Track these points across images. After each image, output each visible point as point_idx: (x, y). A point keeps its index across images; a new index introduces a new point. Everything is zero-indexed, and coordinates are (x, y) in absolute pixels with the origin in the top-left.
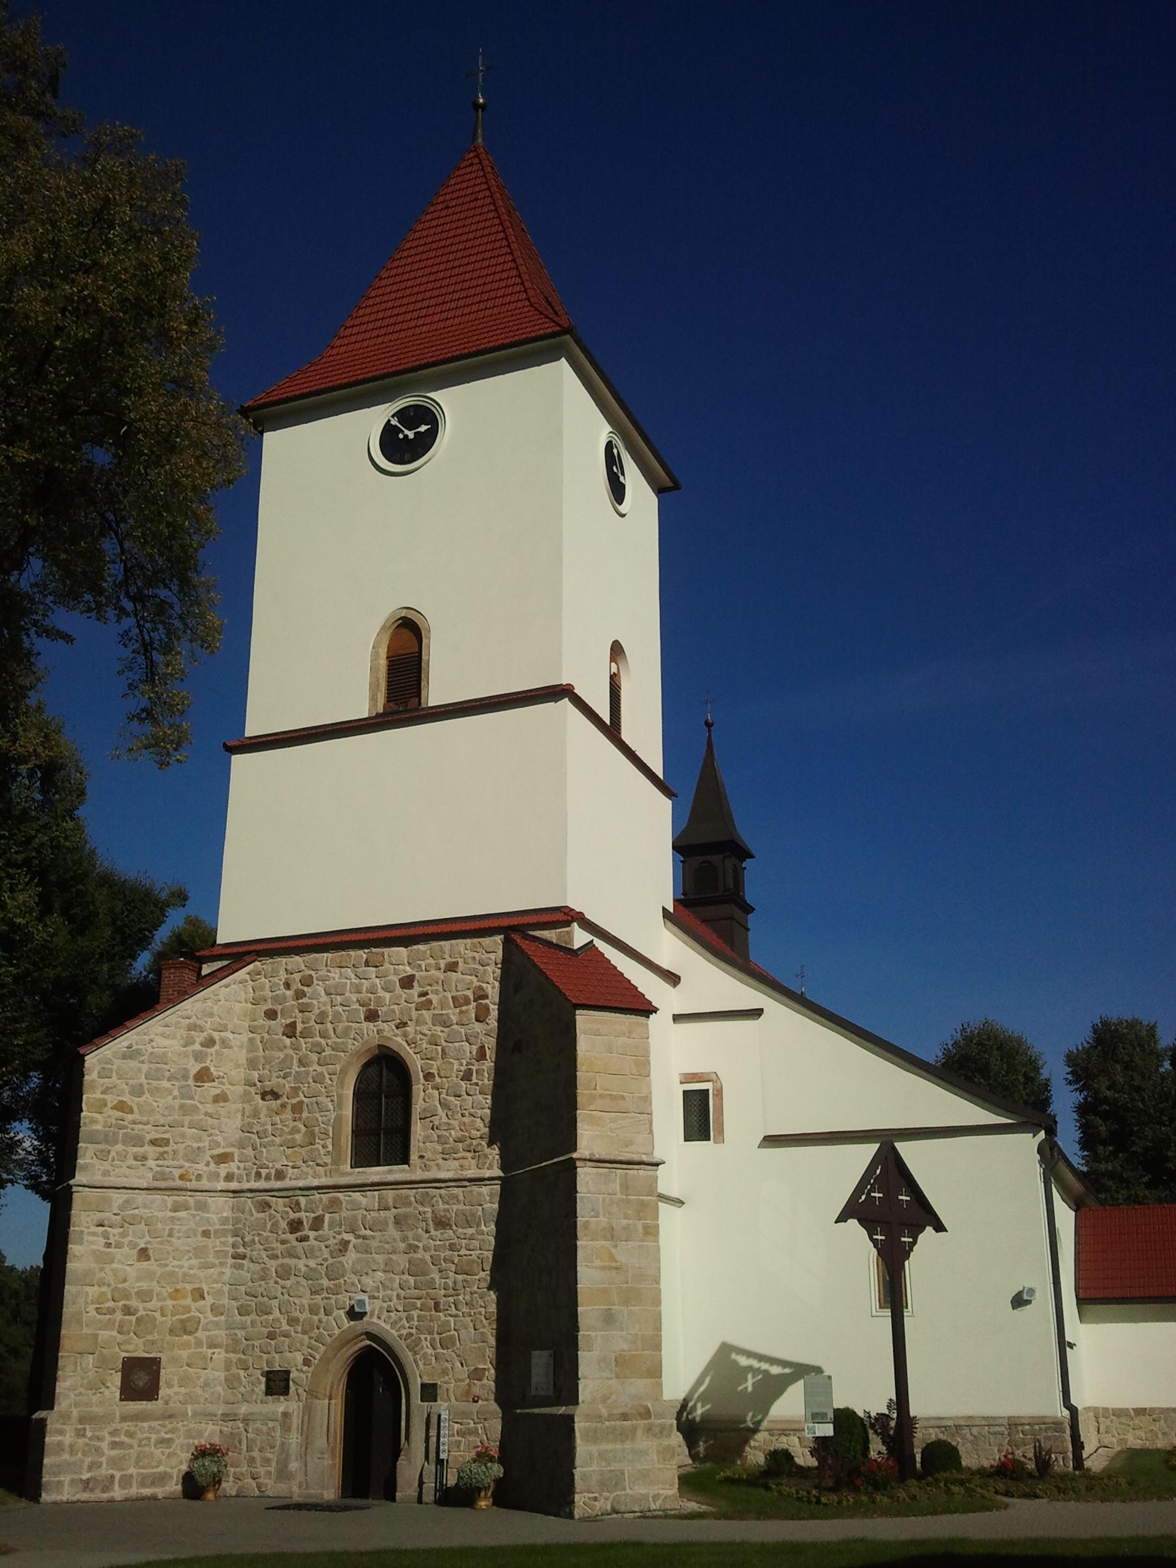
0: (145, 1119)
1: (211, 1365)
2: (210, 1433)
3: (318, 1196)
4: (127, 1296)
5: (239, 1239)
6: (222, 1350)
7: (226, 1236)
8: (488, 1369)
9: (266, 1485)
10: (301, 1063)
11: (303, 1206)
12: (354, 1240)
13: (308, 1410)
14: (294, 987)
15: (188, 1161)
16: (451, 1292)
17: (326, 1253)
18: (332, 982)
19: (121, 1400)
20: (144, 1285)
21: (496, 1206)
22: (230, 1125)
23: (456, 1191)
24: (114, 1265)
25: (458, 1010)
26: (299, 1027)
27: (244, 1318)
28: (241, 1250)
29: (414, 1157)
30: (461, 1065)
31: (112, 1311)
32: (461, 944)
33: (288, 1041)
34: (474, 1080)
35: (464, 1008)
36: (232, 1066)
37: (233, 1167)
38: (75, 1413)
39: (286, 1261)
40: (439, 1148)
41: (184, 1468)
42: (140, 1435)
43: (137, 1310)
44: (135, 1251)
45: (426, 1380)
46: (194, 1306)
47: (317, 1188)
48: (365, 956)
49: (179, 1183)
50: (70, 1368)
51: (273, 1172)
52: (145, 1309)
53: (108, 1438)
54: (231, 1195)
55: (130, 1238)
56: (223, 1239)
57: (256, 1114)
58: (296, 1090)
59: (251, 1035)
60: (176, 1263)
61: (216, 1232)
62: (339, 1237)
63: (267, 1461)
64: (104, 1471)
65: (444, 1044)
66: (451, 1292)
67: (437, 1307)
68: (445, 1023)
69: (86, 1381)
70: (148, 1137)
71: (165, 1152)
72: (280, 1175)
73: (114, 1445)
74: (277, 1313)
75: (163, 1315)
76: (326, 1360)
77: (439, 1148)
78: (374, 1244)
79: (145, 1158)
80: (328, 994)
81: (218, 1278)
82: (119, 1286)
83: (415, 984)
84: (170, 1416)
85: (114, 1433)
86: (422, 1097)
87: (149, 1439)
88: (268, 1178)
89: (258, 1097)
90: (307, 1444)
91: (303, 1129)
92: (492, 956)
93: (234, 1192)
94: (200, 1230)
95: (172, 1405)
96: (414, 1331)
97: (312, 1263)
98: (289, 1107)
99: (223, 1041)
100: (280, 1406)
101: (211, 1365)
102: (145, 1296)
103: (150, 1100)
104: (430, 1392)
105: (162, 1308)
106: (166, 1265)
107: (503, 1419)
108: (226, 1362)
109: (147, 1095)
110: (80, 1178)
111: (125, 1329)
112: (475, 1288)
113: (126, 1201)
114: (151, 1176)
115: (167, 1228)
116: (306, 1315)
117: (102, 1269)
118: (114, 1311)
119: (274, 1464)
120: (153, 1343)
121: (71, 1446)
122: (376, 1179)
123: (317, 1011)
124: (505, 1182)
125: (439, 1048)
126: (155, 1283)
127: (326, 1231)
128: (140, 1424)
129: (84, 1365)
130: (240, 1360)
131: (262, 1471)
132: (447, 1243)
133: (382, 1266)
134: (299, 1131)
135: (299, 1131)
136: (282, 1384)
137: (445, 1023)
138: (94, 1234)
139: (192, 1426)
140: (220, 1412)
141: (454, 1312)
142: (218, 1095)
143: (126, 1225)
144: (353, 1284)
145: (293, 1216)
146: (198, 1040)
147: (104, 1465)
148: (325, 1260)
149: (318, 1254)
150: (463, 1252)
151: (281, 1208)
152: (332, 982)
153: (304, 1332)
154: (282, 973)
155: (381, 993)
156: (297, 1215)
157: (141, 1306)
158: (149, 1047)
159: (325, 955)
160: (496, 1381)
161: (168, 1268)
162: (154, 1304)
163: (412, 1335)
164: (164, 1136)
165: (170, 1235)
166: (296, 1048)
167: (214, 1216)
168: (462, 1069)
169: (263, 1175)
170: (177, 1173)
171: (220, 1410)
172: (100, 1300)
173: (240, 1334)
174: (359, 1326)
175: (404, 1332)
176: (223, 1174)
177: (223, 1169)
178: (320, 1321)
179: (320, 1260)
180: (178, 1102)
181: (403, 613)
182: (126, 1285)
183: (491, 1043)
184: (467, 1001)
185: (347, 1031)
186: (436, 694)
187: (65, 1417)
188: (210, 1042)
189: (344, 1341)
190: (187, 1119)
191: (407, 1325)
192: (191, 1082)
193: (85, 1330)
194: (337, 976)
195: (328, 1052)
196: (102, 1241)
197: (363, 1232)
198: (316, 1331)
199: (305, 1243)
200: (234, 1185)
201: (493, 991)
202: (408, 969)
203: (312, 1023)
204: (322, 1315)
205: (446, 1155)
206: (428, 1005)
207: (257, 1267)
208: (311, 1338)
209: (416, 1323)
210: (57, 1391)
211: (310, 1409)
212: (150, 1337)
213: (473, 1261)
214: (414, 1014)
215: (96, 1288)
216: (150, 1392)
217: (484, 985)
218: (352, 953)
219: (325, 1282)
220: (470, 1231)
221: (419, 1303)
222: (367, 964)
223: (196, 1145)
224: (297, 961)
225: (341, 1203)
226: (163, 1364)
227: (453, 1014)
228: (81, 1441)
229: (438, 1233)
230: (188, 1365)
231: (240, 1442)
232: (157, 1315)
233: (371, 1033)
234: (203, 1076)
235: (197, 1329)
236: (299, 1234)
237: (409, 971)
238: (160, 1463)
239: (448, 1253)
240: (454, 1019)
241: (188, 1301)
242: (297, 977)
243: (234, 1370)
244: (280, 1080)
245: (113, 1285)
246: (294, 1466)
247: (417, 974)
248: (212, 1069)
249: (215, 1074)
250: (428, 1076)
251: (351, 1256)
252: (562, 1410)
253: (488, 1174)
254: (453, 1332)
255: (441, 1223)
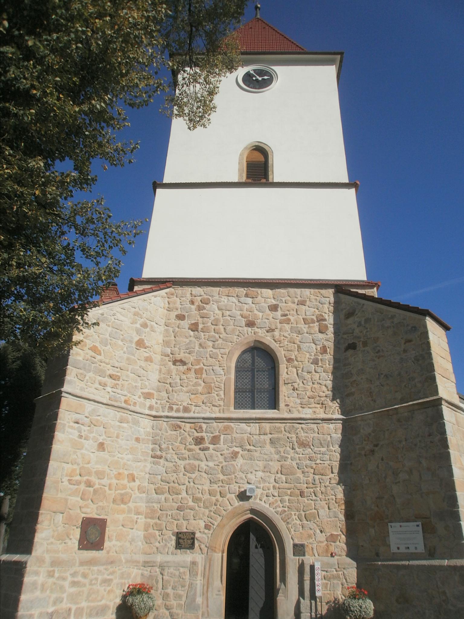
0: (107, 361)
1: (136, 527)
2: (135, 576)
3: (215, 424)
4: (89, 473)
5: (157, 446)
6: (143, 517)
7: (148, 444)
8: (340, 535)
9: (178, 615)
10: (200, 345)
11: (204, 429)
12: (241, 452)
13: (209, 561)
14: (196, 304)
15: (129, 392)
16: (311, 485)
17: (221, 459)
18: (222, 303)
19: (79, 549)
20: (100, 467)
21: (340, 435)
22: (154, 375)
23: (315, 426)
24: (83, 451)
25: (307, 326)
26: (201, 326)
27: (160, 496)
28: (159, 453)
29: (282, 405)
30: (311, 355)
31: (78, 483)
32: (307, 292)
33: (192, 333)
34: (320, 364)
35: (311, 325)
36: (156, 339)
37: (153, 402)
38: (48, 558)
39: (192, 462)
40: (299, 401)
41: (118, 601)
42: (91, 577)
43: (94, 484)
44: (96, 444)
45: (297, 542)
46: (128, 485)
47: (215, 419)
48: (245, 292)
49: (123, 405)
50: (46, 523)
51: (181, 407)
52: (99, 484)
53: (70, 579)
54: (152, 418)
55: (94, 435)
56: (147, 445)
57: (169, 372)
58: (198, 362)
59: (166, 328)
60: (120, 455)
61: (143, 439)
62: (231, 449)
63: (180, 597)
64: (65, 605)
65: (299, 343)
66: (311, 485)
67: (302, 494)
68: (299, 333)
69: (56, 534)
70: (108, 373)
71: (118, 384)
72: (186, 410)
73: (74, 584)
74: (184, 494)
75: (110, 489)
76: (221, 526)
77: (299, 401)
78: (257, 454)
79: (105, 385)
80: (219, 309)
81: (143, 467)
82: (86, 466)
83: (279, 309)
84: (112, 562)
85: (74, 575)
86: (285, 372)
87: (96, 579)
88: (178, 410)
89: (170, 364)
90: (208, 584)
91: (203, 384)
92: (328, 299)
93: (155, 417)
94: (135, 436)
95: (111, 554)
96: (286, 509)
97: (211, 464)
98: (193, 370)
99: (152, 327)
100: (187, 557)
101: (136, 527)
102: (100, 475)
103: (111, 350)
104: (299, 549)
105: (110, 485)
106: (114, 456)
107: (357, 568)
108: (145, 525)
109: (109, 346)
110: (66, 388)
111: (86, 497)
112: (328, 483)
113: (94, 410)
114: (108, 397)
115: (116, 432)
116: (207, 496)
117: (75, 453)
118: (80, 483)
119: (184, 599)
120: (103, 508)
121: (43, 585)
122: (258, 416)
123: (212, 318)
124: (345, 423)
125: (296, 345)
126: (107, 467)
127: (221, 445)
128: (92, 568)
129: (56, 521)
130: (156, 524)
131: (174, 603)
132: (308, 456)
133: (262, 468)
134: (200, 385)
135: (200, 385)
136: (189, 542)
137: (299, 333)
138: (72, 427)
139: (124, 570)
140: (141, 561)
141: (314, 498)
142: (147, 357)
143: (92, 426)
144: (242, 478)
145: (196, 434)
146: (139, 322)
147: (65, 600)
148: (221, 463)
149: (216, 459)
150: (318, 461)
151: (188, 429)
152: (222, 303)
153: (206, 507)
154: (188, 295)
155: (256, 312)
156: (199, 435)
157: (97, 481)
158: (113, 318)
159: (218, 289)
160: (347, 544)
161: (116, 458)
162: (105, 481)
163: (285, 511)
164: (119, 374)
165: (117, 437)
166: (197, 338)
167: (142, 430)
168: (312, 357)
169: (175, 409)
170: (123, 398)
171: (141, 558)
172: (71, 474)
173: (156, 506)
174: (247, 505)
175: (280, 509)
176: (148, 405)
177: (148, 403)
178: (217, 500)
179: (217, 463)
180: (126, 356)
181: (257, 144)
182: (89, 466)
183: (330, 345)
184: (313, 322)
185: (233, 330)
186: (278, 174)
187: (41, 561)
188: (145, 325)
189: (234, 514)
190: (130, 367)
191: (281, 505)
192: (134, 345)
193: (60, 495)
194: (226, 301)
195: (220, 341)
196: (77, 433)
197: (248, 447)
198: (214, 506)
199: (206, 452)
200: (154, 413)
201: (330, 320)
202: (273, 301)
203: (209, 324)
204: (218, 496)
205: (302, 405)
206: (288, 321)
207: (171, 465)
208: (210, 511)
209: (288, 504)
210: (36, 540)
211: (210, 560)
212: (101, 504)
213: (326, 467)
214: (279, 326)
215: (70, 465)
216: (98, 545)
217: (324, 314)
218: (236, 289)
219: (221, 477)
220: (323, 450)
221: (289, 492)
222: (247, 296)
223: (134, 384)
224: (198, 290)
225: (233, 428)
226: (108, 523)
227: (304, 328)
228: (51, 580)
229: (301, 450)
230: (123, 526)
231: (157, 582)
232: (107, 488)
233: (250, 334)
234: (140, 344)
235: (130, 501)
236: (201, 446)
237: (274, 302)
238: (102, 598)
239: (308, 462)
240: (305, 330)
241: (125, 482)
242: (199, 298)
243: (151, 531)
244: (187, 354)
245: (81, 465)
246: (199, 600)
247: (280, 304)
248: (145, 341)
249: (147, 344)
250: (289, 360)
251: (240, 461)
252: (16, 557)
253: (334, 417)
254: (314, 511)
255: (303, 444)
